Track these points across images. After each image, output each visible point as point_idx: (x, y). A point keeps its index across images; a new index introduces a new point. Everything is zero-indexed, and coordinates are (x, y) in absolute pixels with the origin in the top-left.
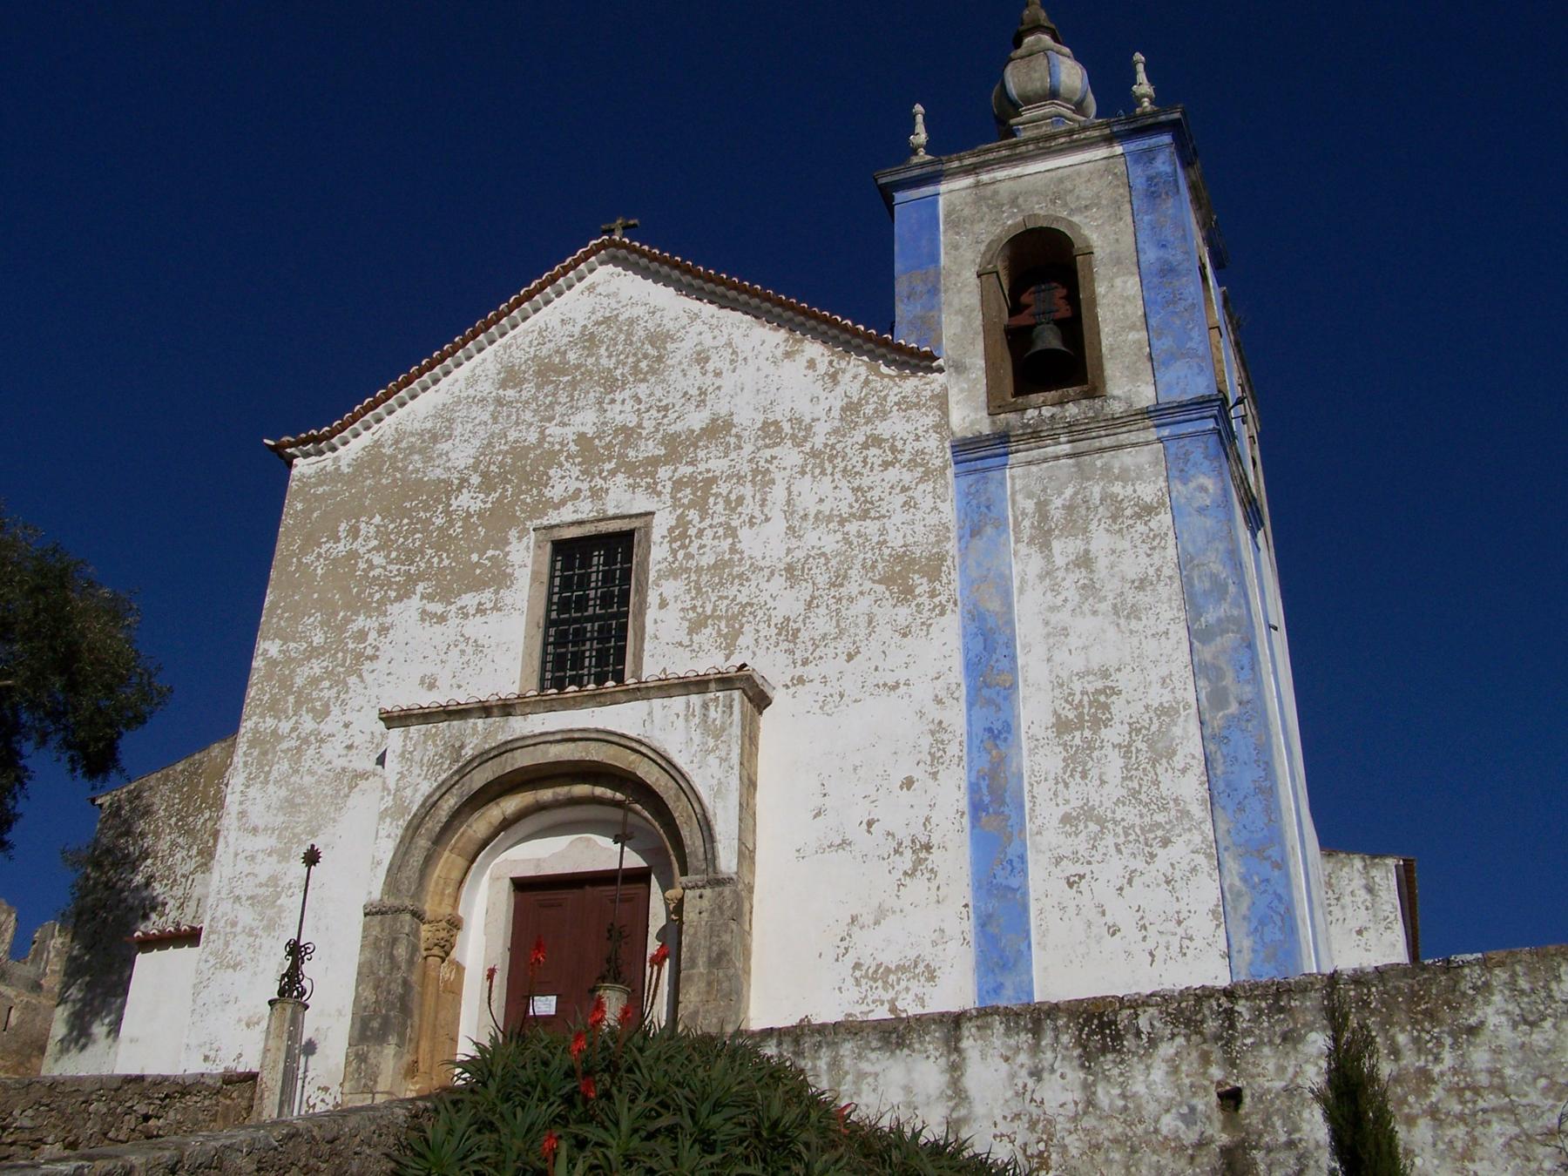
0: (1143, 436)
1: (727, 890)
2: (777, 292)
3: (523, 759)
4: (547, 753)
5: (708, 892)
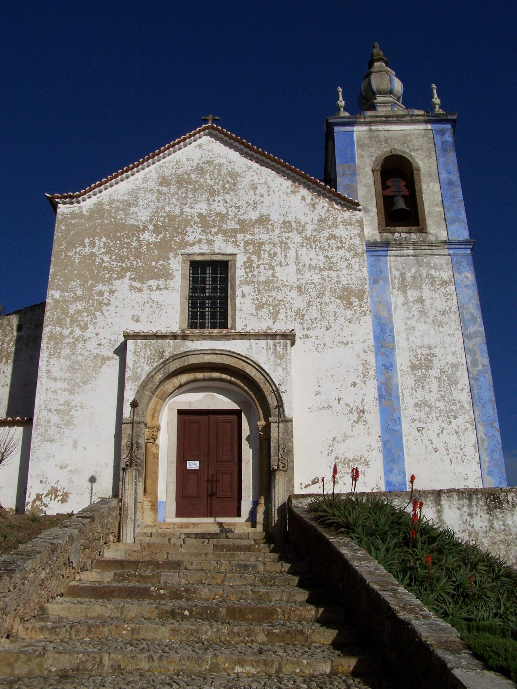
0: (442, 252)
1: (289, 425)
3: (193, 360)
4: (203, 358)
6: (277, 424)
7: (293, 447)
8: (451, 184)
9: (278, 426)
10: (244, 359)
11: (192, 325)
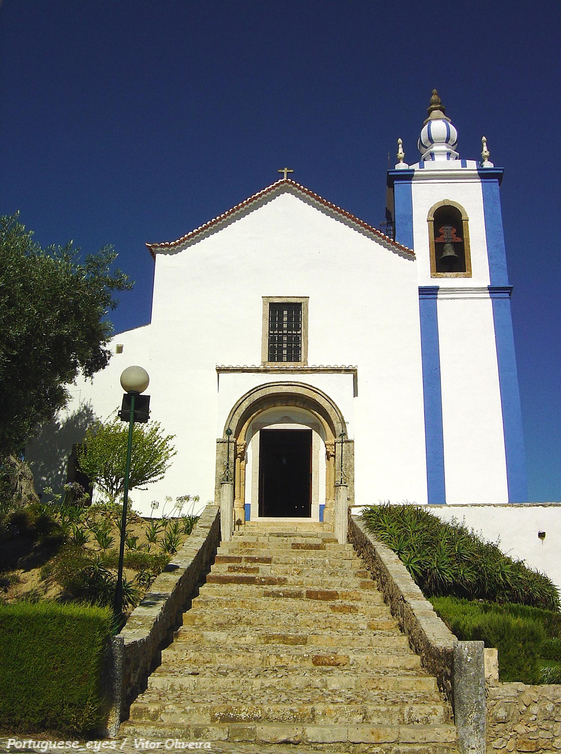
1: (351, 444)
2: (355, 217)
4: (282, 389)
6: (341, 444)
7: (354, 463)
9: (342, 445)
10: (315, 389)
11: (271, 359)
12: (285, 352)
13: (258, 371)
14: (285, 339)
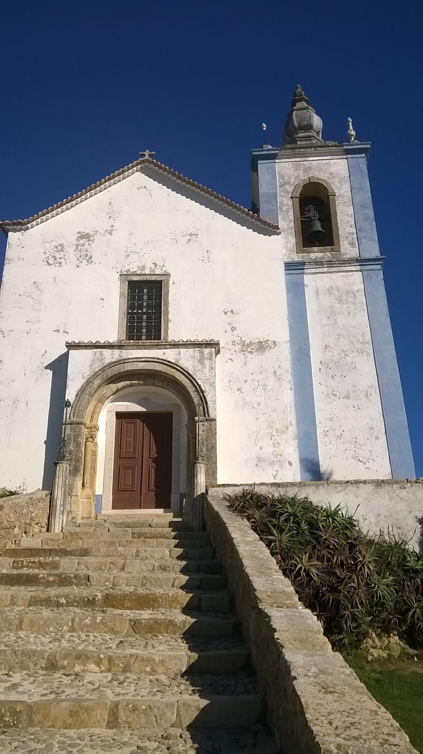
0: (354, 268)
1: (213, 423)
3: (129, 367)
4: (137, 365)
5: (206, 423)
7: (216, 443)
8: (363, 206)
12: (144, 330)
13: (110, 346)
14: (145, 317)
